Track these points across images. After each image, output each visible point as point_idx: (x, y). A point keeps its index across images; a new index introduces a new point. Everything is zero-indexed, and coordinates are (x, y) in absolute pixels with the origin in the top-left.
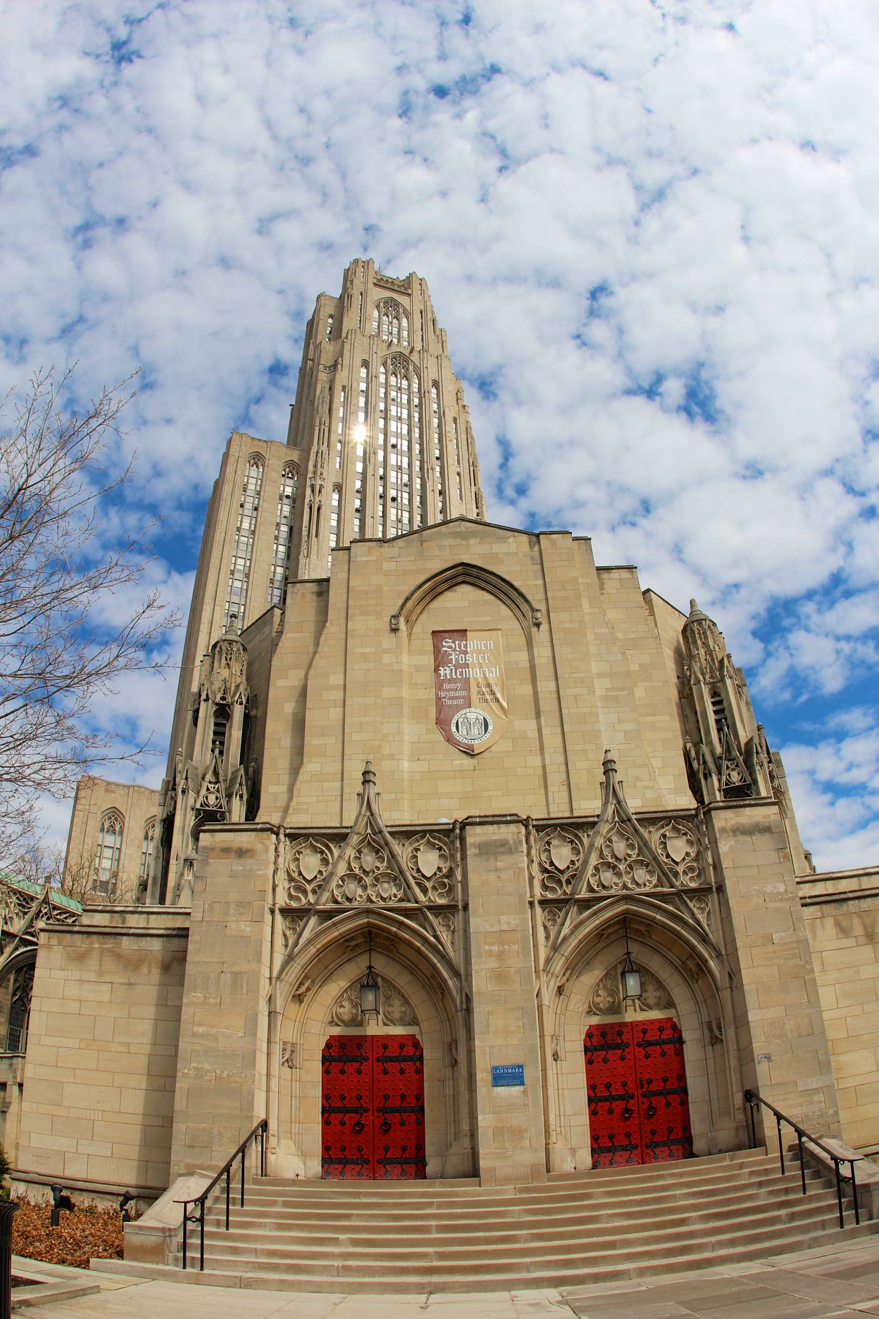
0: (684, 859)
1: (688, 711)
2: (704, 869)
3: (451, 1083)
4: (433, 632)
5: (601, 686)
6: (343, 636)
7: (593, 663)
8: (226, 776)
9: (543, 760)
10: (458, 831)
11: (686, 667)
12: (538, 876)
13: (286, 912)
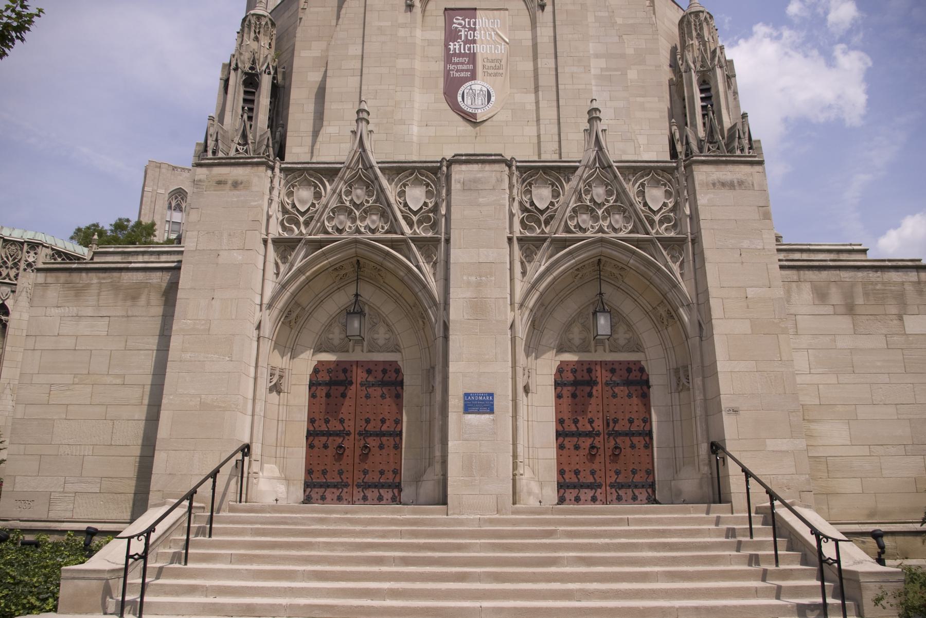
0: (661, 209)
1: (676, 97)
2: (680, 219)
3: (428, 408)
4: (446, 9)
5: (596, 65)
6: (362, 10)
7: (591, 44)
8: (255, 138)
9: (539, 130)
10: (445, 169)
11: (678, 57)
12: (518, 215)
13: (277, 242)
